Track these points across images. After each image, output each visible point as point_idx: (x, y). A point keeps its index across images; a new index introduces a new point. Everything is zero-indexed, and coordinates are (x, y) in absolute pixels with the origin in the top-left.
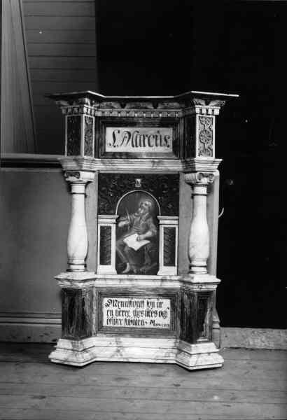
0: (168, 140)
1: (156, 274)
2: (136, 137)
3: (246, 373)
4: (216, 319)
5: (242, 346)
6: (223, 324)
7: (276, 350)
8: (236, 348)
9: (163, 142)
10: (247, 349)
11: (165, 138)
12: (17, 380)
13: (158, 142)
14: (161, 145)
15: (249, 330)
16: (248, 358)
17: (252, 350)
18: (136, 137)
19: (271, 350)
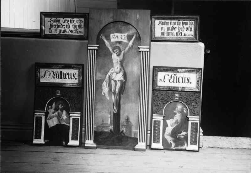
0: (75, 75)
1: (137, 139)
2: (57, 73)
3: (221, 161)
4: (201, 131)
5: (216, 146)
6: (205, 134)
7: (236, 148)
8: (212, 147)
9: (73, 77)
10: (218, 148)
11: (188, 79)
12: (84, 163)
13: (70, 77)
14: (71, 79)
15: (218, 138)
16: (220, 152)
17: (221, 148)
18: (57, 73)
19: (232, 148)
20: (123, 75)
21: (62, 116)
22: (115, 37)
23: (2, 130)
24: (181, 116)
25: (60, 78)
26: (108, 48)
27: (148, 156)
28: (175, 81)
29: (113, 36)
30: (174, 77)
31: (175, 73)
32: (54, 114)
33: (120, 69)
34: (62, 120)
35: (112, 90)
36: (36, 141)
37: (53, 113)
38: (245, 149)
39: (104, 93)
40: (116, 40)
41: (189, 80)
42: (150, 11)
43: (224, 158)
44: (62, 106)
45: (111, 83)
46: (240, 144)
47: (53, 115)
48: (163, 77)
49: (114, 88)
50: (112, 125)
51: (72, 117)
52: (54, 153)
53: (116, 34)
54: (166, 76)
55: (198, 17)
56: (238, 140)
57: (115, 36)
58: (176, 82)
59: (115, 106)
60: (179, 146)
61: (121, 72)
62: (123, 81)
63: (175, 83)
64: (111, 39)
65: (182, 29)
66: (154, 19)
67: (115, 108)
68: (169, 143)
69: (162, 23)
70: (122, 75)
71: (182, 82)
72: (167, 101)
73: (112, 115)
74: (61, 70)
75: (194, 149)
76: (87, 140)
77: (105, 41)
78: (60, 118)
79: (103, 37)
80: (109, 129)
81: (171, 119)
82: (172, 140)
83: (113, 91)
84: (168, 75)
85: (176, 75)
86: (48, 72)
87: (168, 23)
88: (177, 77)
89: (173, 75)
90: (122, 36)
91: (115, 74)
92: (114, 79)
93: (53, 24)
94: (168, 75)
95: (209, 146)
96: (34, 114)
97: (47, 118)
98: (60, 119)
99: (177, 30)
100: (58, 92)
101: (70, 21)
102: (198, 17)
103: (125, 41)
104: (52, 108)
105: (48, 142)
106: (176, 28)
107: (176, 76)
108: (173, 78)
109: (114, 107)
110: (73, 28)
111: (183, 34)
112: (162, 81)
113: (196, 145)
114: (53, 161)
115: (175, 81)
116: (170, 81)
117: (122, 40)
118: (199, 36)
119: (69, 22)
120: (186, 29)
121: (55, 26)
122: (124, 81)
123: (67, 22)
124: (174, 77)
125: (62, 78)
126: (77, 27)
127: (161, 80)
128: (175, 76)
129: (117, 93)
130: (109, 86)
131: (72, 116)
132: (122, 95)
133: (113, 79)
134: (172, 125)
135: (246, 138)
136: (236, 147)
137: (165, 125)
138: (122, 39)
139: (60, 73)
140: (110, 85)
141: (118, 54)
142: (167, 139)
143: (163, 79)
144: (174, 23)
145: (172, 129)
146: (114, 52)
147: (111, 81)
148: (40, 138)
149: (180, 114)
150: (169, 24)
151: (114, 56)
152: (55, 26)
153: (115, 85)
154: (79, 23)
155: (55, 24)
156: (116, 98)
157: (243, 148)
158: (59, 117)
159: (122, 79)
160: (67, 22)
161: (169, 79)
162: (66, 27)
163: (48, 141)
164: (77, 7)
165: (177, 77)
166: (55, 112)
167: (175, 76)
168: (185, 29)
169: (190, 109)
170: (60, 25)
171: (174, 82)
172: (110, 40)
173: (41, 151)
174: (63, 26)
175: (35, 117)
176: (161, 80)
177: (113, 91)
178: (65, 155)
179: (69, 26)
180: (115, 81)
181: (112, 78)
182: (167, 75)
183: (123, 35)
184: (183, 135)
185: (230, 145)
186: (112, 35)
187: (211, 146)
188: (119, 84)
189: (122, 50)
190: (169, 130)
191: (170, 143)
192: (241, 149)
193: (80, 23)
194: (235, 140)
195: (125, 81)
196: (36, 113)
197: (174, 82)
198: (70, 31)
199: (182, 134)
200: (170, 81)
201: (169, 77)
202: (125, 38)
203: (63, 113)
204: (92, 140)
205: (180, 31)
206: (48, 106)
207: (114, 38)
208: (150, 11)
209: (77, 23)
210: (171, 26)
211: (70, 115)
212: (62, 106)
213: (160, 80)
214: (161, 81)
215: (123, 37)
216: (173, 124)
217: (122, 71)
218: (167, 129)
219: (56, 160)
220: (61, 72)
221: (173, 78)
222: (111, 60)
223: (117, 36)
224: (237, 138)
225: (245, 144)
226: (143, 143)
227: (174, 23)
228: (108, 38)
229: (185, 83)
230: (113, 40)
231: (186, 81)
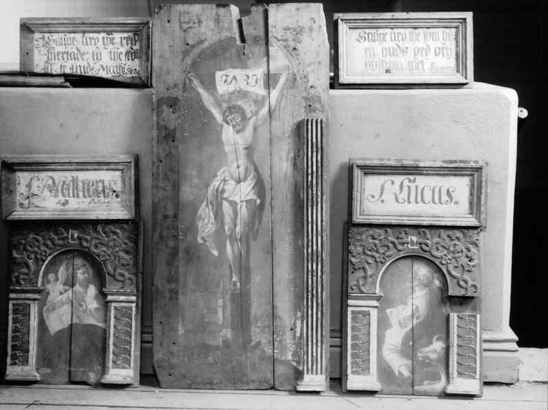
11: (448, 191)
20: (253, 188)
21: (85, 302)
22: (229, 79)
23: (332, 348)
24: (429, 296)
25: (74, 196)
26: (209, 112)
28: (413, 199)
29: (222, 78)
30: (409, 188)
31: (412, 177)
32: (64, 296)
33: (246, 170)
34: (85, 311)
35: (227, 228)
36: (13, 372)
37: (61, 293)
39: (202, 238)
40: (231, 88)
41: (452, 194)
42: (472, 13)
44: (84, 274)
45: (222, 208)
47: (60, 297)
48: (379, 188)
49: (231, 224)
51: (114, 305)
53: (232, 72)
54: (388, 185)
55: (469, 16)
57: (227, 76)
58: (417, 202)
59: (234, 274)
60: (426, 382)
61: (249, 178)
62: (255, 201)
63: (421, 204)
64: (218, 87)
65: (424, 51)
67: (234, 279)
68: (397, 373)
69: (366, 36)
70: (253, 184)
71: (430, 200)
72: (388, 256)
73: (228, 297)
74: (75, 174)
75: (467, 389)
76: (308, 373)
77: (201, 91)
78: (81, 305)
79: (196, 82)
80: (221, 340)
81: (400, 307)
82: (403, 365)
83: (228, 233)
84: (393, 183)
85: (414, 181)
86: (39, 179)
87: (384, 35)
88: (417, 187)
89: (406, 183)
90: (248, 77)
91: (233, 183)
92: (231, 199)
93: (56, 51)
94: (393, 183)
95: (537, 380)
96: (8, 295)
97: (45, 308)
98: (81, 309)
99: (410, 56)
100: (72, 236)
101: (101, 41)
102: (469, 16)
103: (260, 91)
104: (57, 279)
106: (407, 48)
107: (415, 184)
108: (405, 189)
109: (232, 277)
110: (111, 59)
111: (427, 66)
112: (376, 198)
113: (474, 378)
115: (413, 199)
116: (397, 200)
117: (249, 89)
119: (100, 44)
120: (435, 52)
121: (61, 56)
122: (258, 202)
123: (95, 44)
124: (409, 188)
125: (78, 197)
126: (123, 57)
127: (373, 197)
128: (413, 186)
130: (215, 219)
131: (12, 299)
132: (252, 242)
133: (226, 199)
134: (402, 321)
137: (384, 323)
138: (248, 84)
139: (73, 181)
140: (219, 215)
141: (238, 128)
142: (391, 364)
143: (377, 195)
144: (400, 37)
145: (403, 334)
146: (228, 123)
147: (222, 202)
148: (26, 362)
149: (424, 292)
150: (388, 37)
151: (228, 133)
152: (61, 56)
153: (232, 216)
154: (127, 44)
155: (61, 49)
156: (236, 250)
158: (75, 304)
159: (252, 196)
160: (93, 42)
161: (395, 194)
162: (91, 59)
165: (417, 187)
166: (66, 291)
167: (413, 186)
168: (433, 51)
169: (453, 277)
170: (76, 51)
171: (409, 202)
172: (215, 88)
173: (65, 402)
174: (83, 55)
175: (10, 306)
176: (373, 197)
177: (228, 233)
179: (101, 54)
180: (233, 204)
181: (225, 196)
182: (391, 182)
183: (250, 73)
184: (435, 351)
186: (219, 74)
187: (539, 380)
188: (244, 212)
189: (249, 115)
190: (395, 336)
191: (399, 373)
193: (130, 45)
195: (261, 203)
196: (12, 296)
197: (409, 202)
198: (104, 69)
199: (431, 348)
200: (397, 200)
201: (396, 188)
202: (257, 82)
203: (89, 291)
204: (321, 374)
205: (420, 58)
206: (46, 273)
207: (225, 81)
208: (472, 13)
209: (122, 44)
210: (393, 45)
211: (106, 297)
212: (84, 274)
213: (370, 197)
214: (373, 200)
215: (252, 81)
216: (404, 319)
217: (252, 175)
218: (388, 333)
220: (74, 180)
221: (405, 189)
222: (219, 142)
223: (235, 78)
226: (313, 376)
227: (400, 37)
228: (210, 85)
229: (441, 203)
230: (222, 88)
231: (445, 198)
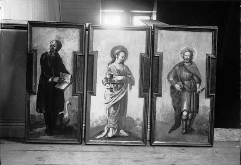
19: (223, 141)
20: (206, 106)
27: (138, 152)
38: (236, 141)
43: (217, 152)
46: (230, 136)
50: (63, 120)
52: (38, 151)
56: (228, 132)
66: (157, 29)
105: (97, 136)
114: (38, 160)
118: (185, 26)
129: (59, 78)
135: (236, 129)
136: (227, 140)
157: (234, 141)
163: (96, 137)
164: (62, 8)
173: (25, 149)
178: (51, 153)
185: (220, 138)
192: (232, 141)
194: (225, 131)
219: (41, 159)
224: (227, 129)
225: (236, 136)
